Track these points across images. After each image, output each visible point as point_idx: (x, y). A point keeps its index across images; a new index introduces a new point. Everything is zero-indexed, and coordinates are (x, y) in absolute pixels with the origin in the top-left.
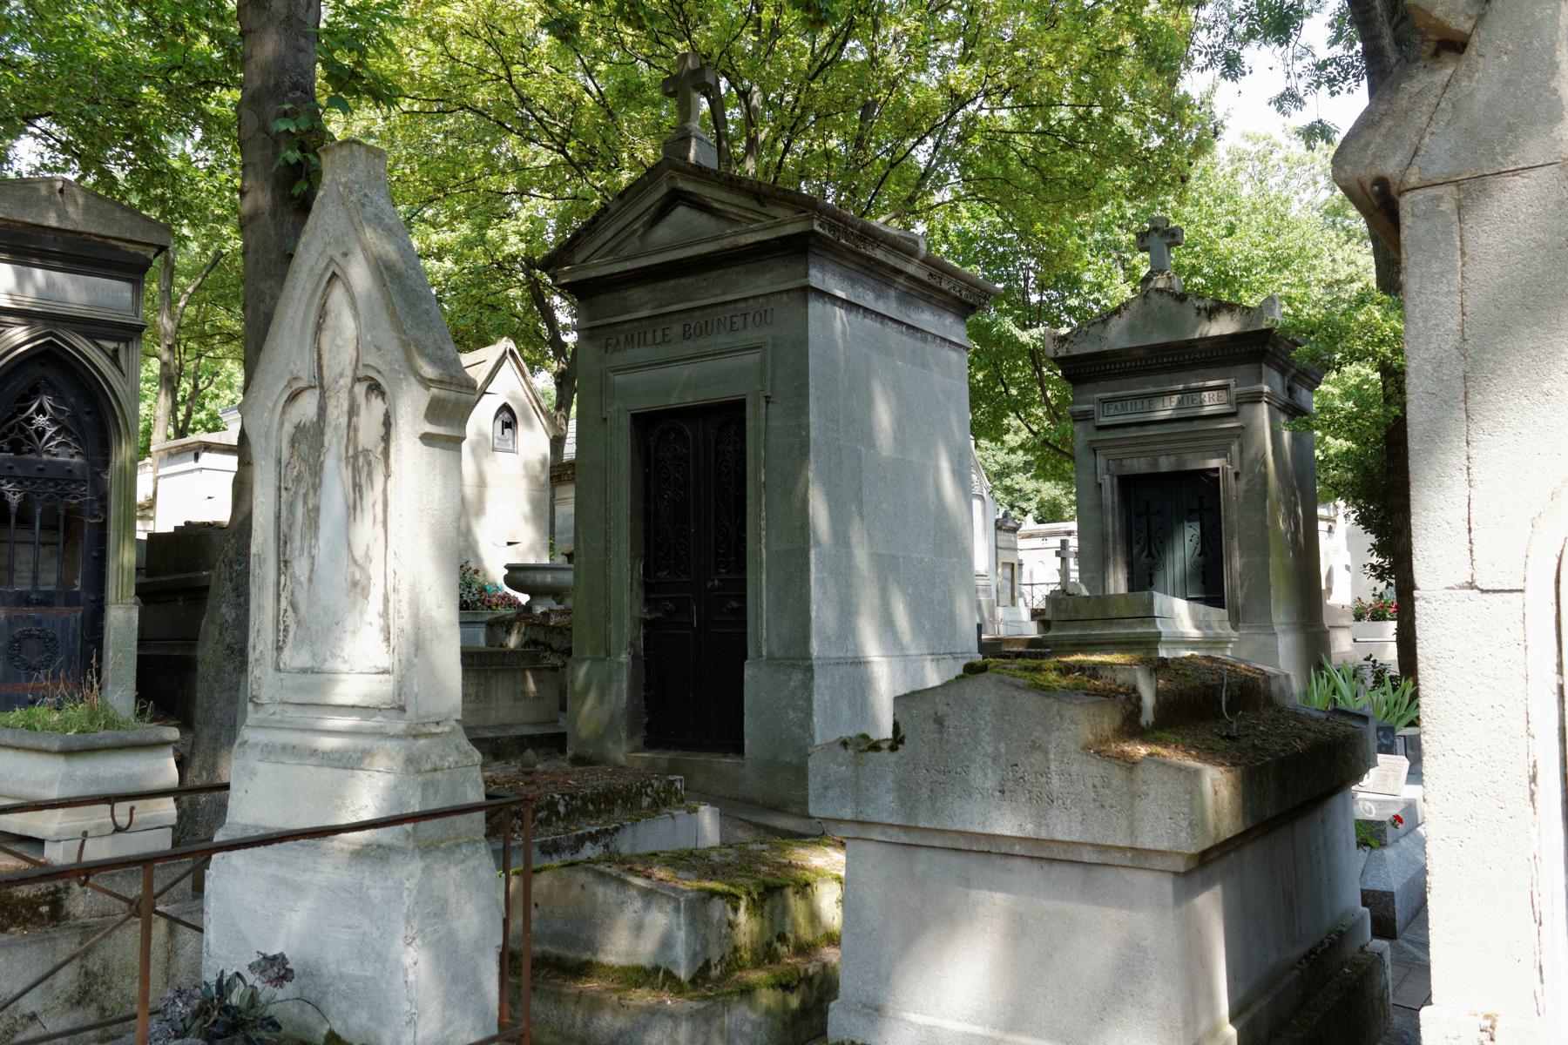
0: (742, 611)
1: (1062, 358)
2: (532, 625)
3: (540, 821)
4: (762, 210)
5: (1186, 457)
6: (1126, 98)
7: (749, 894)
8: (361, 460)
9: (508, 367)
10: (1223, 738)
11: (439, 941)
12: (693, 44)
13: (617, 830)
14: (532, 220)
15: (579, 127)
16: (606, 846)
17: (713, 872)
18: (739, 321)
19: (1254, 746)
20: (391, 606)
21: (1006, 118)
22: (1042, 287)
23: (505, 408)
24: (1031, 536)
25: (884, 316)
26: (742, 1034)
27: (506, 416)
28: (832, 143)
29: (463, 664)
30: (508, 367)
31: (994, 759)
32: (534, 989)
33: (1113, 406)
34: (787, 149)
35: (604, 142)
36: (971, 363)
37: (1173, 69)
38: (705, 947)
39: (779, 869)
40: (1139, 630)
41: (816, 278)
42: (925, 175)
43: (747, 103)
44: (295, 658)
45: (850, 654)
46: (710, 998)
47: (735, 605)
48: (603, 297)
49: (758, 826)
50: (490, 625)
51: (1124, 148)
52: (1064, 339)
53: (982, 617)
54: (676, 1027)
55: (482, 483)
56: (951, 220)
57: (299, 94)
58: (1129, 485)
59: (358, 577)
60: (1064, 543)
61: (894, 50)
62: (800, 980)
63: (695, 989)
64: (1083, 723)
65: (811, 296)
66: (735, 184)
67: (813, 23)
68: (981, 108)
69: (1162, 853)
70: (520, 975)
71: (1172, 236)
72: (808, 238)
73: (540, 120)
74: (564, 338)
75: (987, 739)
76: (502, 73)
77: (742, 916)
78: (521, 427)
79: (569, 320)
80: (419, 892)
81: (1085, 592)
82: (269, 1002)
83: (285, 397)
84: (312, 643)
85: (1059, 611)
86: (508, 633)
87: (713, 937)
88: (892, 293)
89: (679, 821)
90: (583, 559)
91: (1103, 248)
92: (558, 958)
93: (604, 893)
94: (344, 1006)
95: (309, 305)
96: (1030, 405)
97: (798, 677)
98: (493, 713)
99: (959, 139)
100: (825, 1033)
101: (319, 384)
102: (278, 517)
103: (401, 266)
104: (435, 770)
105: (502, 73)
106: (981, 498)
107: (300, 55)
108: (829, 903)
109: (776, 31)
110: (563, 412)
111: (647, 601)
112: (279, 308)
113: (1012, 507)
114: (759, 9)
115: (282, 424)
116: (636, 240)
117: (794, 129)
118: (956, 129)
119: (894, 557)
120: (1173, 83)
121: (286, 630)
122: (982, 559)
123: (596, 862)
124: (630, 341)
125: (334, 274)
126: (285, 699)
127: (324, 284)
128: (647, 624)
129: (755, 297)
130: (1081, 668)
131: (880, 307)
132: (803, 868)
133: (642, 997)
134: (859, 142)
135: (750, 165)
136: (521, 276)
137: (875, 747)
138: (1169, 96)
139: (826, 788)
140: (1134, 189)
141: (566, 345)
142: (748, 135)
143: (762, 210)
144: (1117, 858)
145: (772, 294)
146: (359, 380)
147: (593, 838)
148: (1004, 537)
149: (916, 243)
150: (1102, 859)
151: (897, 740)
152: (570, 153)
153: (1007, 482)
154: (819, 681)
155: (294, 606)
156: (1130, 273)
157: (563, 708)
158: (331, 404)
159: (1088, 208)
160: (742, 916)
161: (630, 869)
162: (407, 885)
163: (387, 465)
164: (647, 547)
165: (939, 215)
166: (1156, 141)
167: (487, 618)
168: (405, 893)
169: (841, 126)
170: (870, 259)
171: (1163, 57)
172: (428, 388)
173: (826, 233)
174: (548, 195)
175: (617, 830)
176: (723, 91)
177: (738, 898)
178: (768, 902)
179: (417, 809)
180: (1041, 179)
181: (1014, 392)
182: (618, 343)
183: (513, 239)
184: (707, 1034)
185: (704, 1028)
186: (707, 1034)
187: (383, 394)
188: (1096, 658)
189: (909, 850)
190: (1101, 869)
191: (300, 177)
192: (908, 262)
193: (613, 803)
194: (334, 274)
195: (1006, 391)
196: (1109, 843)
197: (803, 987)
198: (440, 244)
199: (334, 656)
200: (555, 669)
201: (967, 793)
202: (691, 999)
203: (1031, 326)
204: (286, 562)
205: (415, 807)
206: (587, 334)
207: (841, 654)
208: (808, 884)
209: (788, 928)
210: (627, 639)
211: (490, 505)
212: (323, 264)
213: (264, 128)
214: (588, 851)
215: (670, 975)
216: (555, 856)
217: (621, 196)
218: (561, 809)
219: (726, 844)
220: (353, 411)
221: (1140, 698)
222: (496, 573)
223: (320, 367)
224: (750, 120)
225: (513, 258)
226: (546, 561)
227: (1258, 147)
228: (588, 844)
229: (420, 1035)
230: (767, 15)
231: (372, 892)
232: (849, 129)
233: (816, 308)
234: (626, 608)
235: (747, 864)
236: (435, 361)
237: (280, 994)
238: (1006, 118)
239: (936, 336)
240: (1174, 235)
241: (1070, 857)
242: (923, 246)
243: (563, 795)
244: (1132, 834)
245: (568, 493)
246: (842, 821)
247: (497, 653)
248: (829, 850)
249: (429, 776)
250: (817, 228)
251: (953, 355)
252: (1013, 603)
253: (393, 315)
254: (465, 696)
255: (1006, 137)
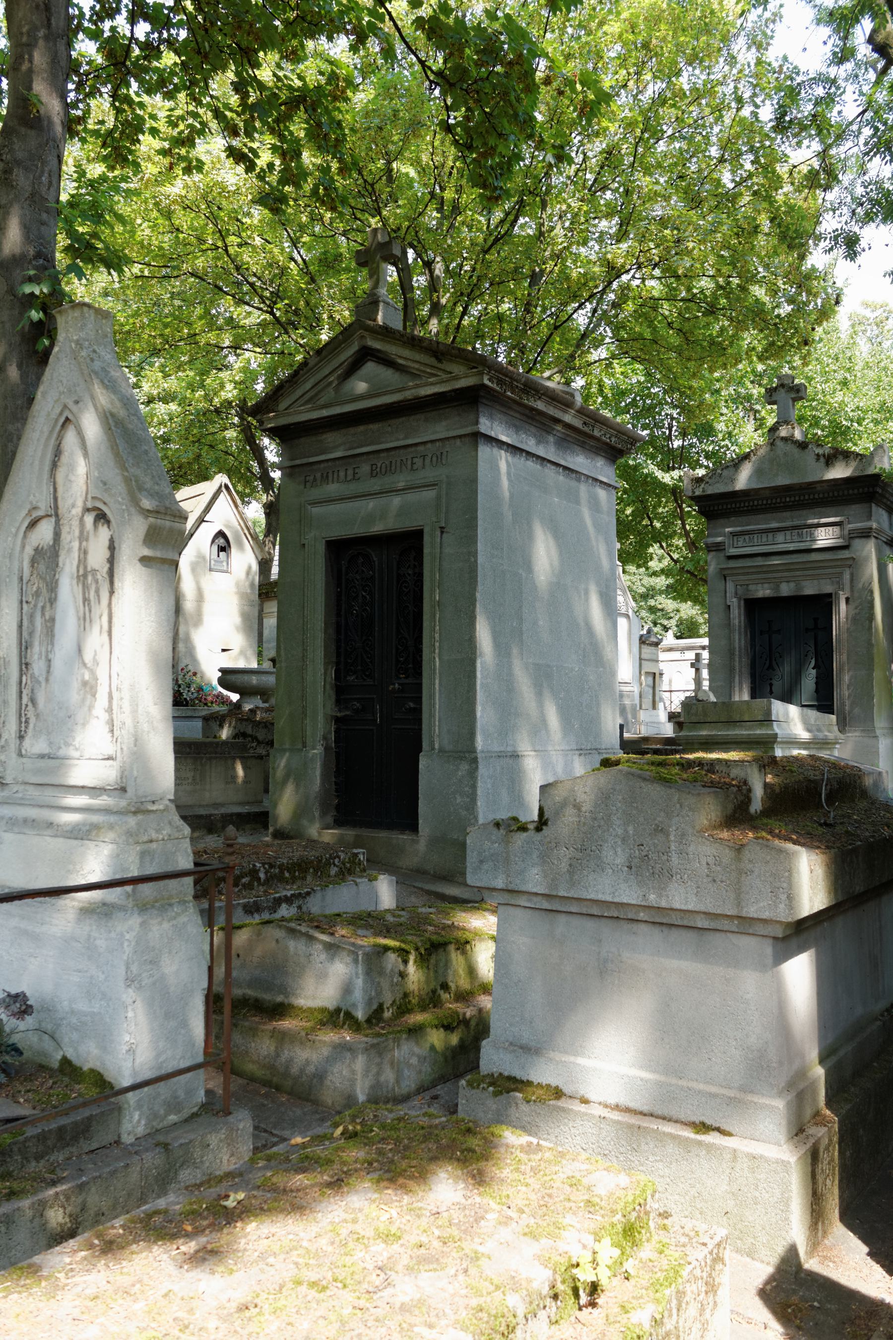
0: (418, 711)
1: (699, 497)
2: (241, 720)
3: (244, 885)
4: (439, 365)
5: (804, 583)
6: (760, 269)
7: (417, 949)
8: (90, 578)
9: (224, 497)
10: (821, 825)
11: (154, 984)
12: (384, 220)
13: (308, 894)
14: (245, 370)
15: (285, 291)
16: (300, 907)
17: (387, 931)
18: (418, 462)
19: (847, 832)
20: (115, 702)
21: (655, 287)
22: (684, 434)
23: (221, 534)
24: (670, 650)
25: (543, 459)
26: (410, 1066)
27: (221, 541)
28: (505, 306)
29: (176, 752)
30: (224, 497)
31: (623, 840)
32: (235, 1025)
33: (741, 539)
34: (464, 313)
35: (307, 303)
36: (621, 499)
37: (803, 245)
38: (379, 993)
39: (443, 929)
40: (758, 732)
41: (485, 425)
42: (584, 336)
43: (431, 272)
44: (35, 745)
45: (509, 749)
46: (382, 1035)
47: (412, 705)
48: (302, 440)
49: (429, 893)
50: (206, 719)
51: (758, 315)
52: (699, 480)
53: (626, 719)
54: (354, 1058)
55: (200, 597)
56: (604, 375)
57: (41, 261)
58: (754, 607)
59: (87, 677)
60: (698, 656)
61: (559, 226)
62: (459, 1022)
63: (370, 1028)
64: (707, 810)
65: (481, 441)
66: (414, 343)
67: (489, 199)
68: (633, 277)
69: (765, 921)
70: (222, 1013)
71: (797, 392)
72: (481, 392)
73: (252, 285)
74: (272, 475)
75: (618, 822)
76: (220, 244)
77: (411, 968)
78: (234, 550)
79: (276, 460)
80: (137, 943)
81: (713, 699)
82: (12, 1032)
83: (26, 524)
84: (49, 733)
85: (690, 715)
86: (221, 726)
87: (385, 984)
88: (551, 439)
89: (361, 887)
90: (283, 664)
91: (737, 399)
92: (257, 1000)
93: (294, 946)
94: (75, 1036)
95: (46, 445)
96: (671, 536)
97: (464, 767)
98: (207, 794)
99: (615, 305)
100: (478, 1067)
101: (55, 513)
102: (20, 626)
103: (122, 413)
104: (151, 841)
105: (220, 244)
106: (627, 616)
107: (43, 228)
108: (484, 958)
109: (456, 209)
110: (271, 538)
111: (338, 702)
112: (21, 448)
113: (655, 624)
114: (442, 189)
115: (23, 547)
116: (331, 391)
117: (468, 294)
118: (612, 296)
119: (549, 666)
120: (802, 257)
121: (27, 722)
122: (625, 669)
123: (290, 920)
124: (325, 479)
125: (67, 419)
126: (26, 780)
127: (58, 427)
128: (337, 720)
129: (432, 441)
130: (700, 763)
131: (541, 451)
132: (464, 929)
133: (329, 1037)
134: (528, 307)
135: (434, 326)
136: (236, 420)
137: (523, 828)
138: (798, 268)
139: (481, 862)
140: (766, 350)
141: (273, 480)
142: (431, 299)
143: (439, 365)
144: (725, 924)
145: (447, 439)
146: (88, 510)
147: (289, 900)
148: (647, 651)
149: (573, 396)
150: (713, 925)
151: (542, 823)
152: (278, 314)
153: (652, 602)
154: (483, 771)
155: (33, 701)
156: (760, 423)
157: (266, 791)
158: (65, 530)
159: (724, 366)
160: (411, 968)
161: (317, 927)
162: (127, 936)
163: (112, 583)
164: (338, 655)
165: (596, 370)
166: (786, 309)
167: (204, 713)
168: (126, 944)
169: (512, 292)
170: (532, 409)
171: (794, 235)
172: (147, 517)
173: (494, 386)
174: (258, 350)
175: (308, 894)
176: (410, 261)
177: (408, 952)
178: (434, 957)
179: (136, 874)
180: (682, 341)
181: (658, 525)
182: (315, 480)
183: (229, 386)
184: (379, 1065)
185: (377, 1060)
186: (379, 1065)
187: (108, 522)
188: (714, 756)
189: (551, 915)
190: (712, 933)
191: (42, 334)
192: (565, 412)
193: (306, 871)
194: (67, 419)
195: (651, 525)
196: (719, 912)
197: (462, 1027)
198: (160, 392)
199: (67, 745)
200: (260, 757)
201: (600, 867)
202: (367, 1036)
203: (674, 469)
204: (27, 664)
205: (134, 872)
206: (289, 471)
207: (502, 749)
208: (467, 942)
209: (450, 978)
210: (320, 734)
211: (207, 618)
212: (57, 410)
213: (12, 291)
214: (284, 911)
215: (349, 1016)
216: (256, 916)
217: (319, 352)
218: (262, 875)
219: (400, 908)
220: (83, 537)
221: (750, 790)
222: (212, 676)
223: (56, 499)
224: (433, 285)
225: (228, 403)
226: (254, 665)
227: (876, 314)
228: (284, 905)
229: (138, 1061)
230: (449, 195)
231: (98, 942)
232: (519, 295)
233: (484, 451)
234: (320, 707)
235: (417, 923)
236: (152, 495)
237: (22, 1025)
238: (655, 287)
239: (588, 477)
240: (798, 391)
241: (685, 923)
242: (579, 399)
243: (263, 864)
244: (739, 905)
245: (272, 607)
246: (494, 889)
247: (211, 743)
248: (486, 914)
249: (146, 846)
250: (486, 382)
251: (602, 493)
252: (654, 707)
253: (117, 455)
254: (177, 778)
255: (653, 303)
